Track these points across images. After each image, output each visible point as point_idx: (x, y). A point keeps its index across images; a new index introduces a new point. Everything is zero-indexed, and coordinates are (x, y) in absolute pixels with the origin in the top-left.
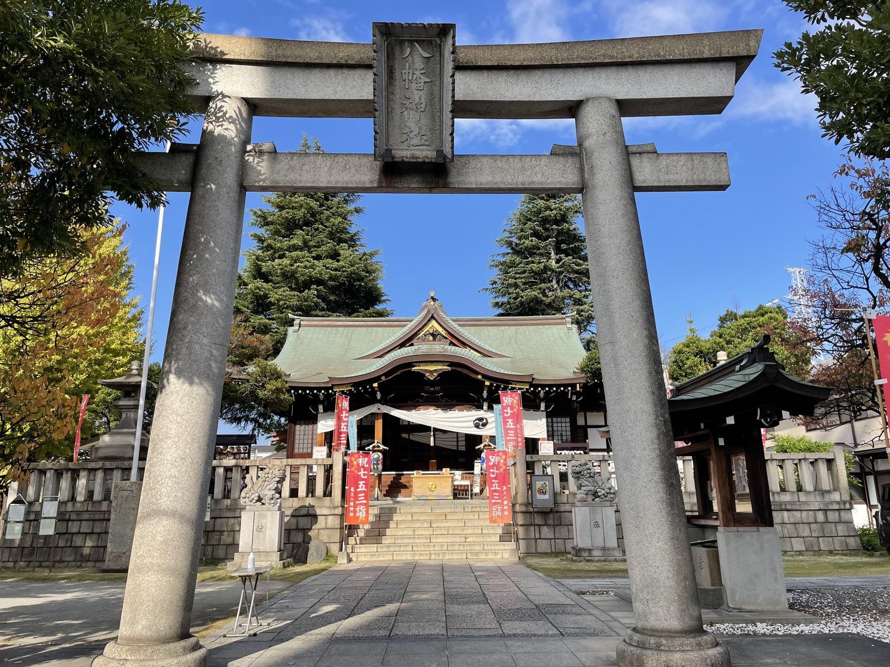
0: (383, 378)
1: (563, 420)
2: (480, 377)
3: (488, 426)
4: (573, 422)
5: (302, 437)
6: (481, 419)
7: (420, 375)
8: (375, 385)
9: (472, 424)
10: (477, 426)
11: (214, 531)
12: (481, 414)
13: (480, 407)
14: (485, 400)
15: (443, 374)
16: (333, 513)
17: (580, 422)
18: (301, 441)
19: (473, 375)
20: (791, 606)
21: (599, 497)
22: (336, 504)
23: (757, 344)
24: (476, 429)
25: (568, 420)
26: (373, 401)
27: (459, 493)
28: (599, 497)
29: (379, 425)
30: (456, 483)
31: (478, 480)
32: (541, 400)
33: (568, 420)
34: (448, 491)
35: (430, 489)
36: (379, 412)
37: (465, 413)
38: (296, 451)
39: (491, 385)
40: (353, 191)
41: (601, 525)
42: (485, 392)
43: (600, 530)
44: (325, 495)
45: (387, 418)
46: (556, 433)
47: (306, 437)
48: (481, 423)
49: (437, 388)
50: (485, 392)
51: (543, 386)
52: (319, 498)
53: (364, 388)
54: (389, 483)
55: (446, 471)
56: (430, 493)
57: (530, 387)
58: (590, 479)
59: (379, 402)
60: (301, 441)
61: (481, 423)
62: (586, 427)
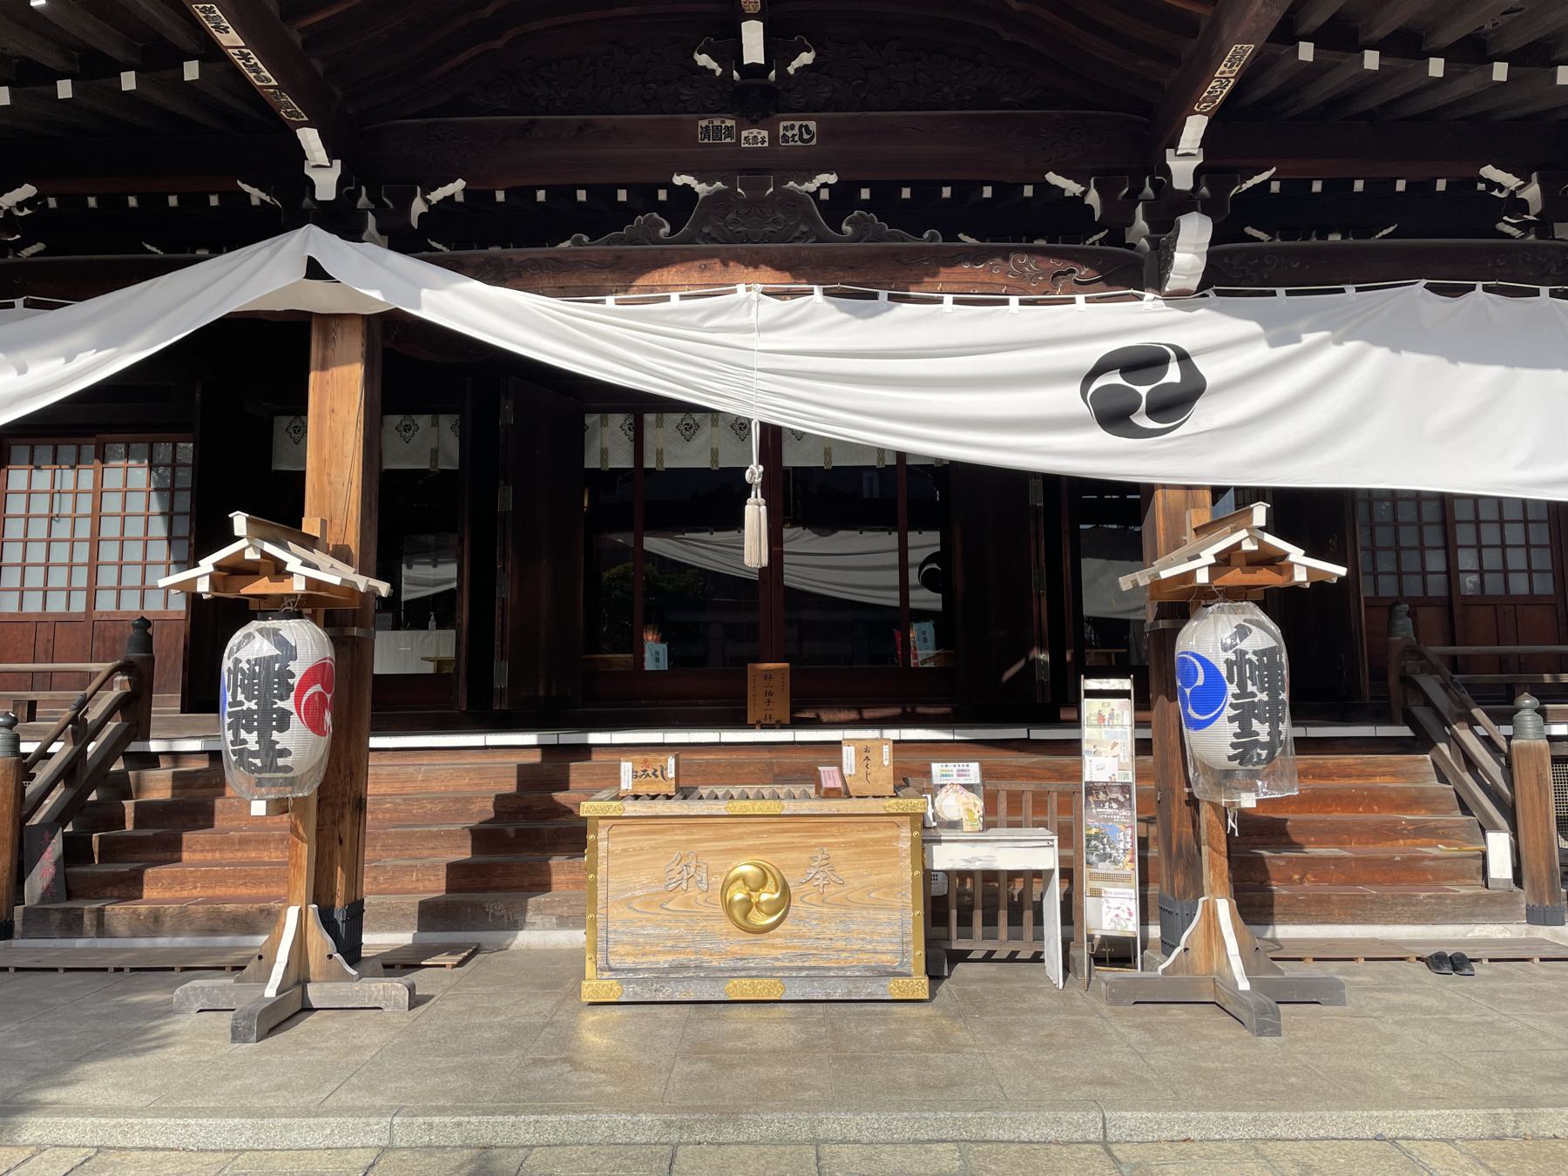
3: (1203, 416)
5: (39, 529)
6: (1144, 362)
9: (1070, 400)
10: (1114, 416)
12: (1140, 319)
13: (1135, 272)
18: (37, 553)
24: (1100, 438)
26: (292, 208)
27: (964, 917)
29: (337, 397)
30: (947, 857)
31: (1117, 829)
34: (892, 930)
35: (740, 916)
36: (317, 298)
37: (1015, 317)
40: (840, 766)
42: (1194, 129)
45: (412, 362)
46: (1433, 536)
47: (62, 530)
48: (1144, 390)
49: (796, 130)
50: (1194, 129)
54: (484, 809)
55: (863, 749)
56: (738, 944)
59: (341, 220)
60: (37, 553)
61: (1144, 390)
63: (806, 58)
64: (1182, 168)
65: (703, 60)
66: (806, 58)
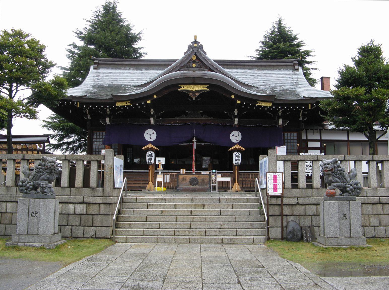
0: (155, 96)
1: (292, 134)
2: (233, 97)
4: (299, 137)
7: (186, 94)
8: (149, 102)
11: (6, 213)
14: (236, 117)
15: (202, 94)
16: (105, 201)
17: (304, 138)
19: (227, 96)
20: (6, 163)
21: (347, 192)
22: (387, 237)
23: (235, 164)
25: (295, 134)
28: (347, 192)
32: (279, 117)
33: (295, 134)
38: (203, 167)
39: (242, 103)
41: (348, 217)
43: (347, 221)
44: (98, 187)
50: (236, 110)
51: (283, 105)
52: (93, 189)
53: (140, 104)
57: (273, 105)
58: (340, 176)
62: (307, 141)
63: (199, 99)
64: (236, 114)
65: (189, 99)
66: (199, 99)
